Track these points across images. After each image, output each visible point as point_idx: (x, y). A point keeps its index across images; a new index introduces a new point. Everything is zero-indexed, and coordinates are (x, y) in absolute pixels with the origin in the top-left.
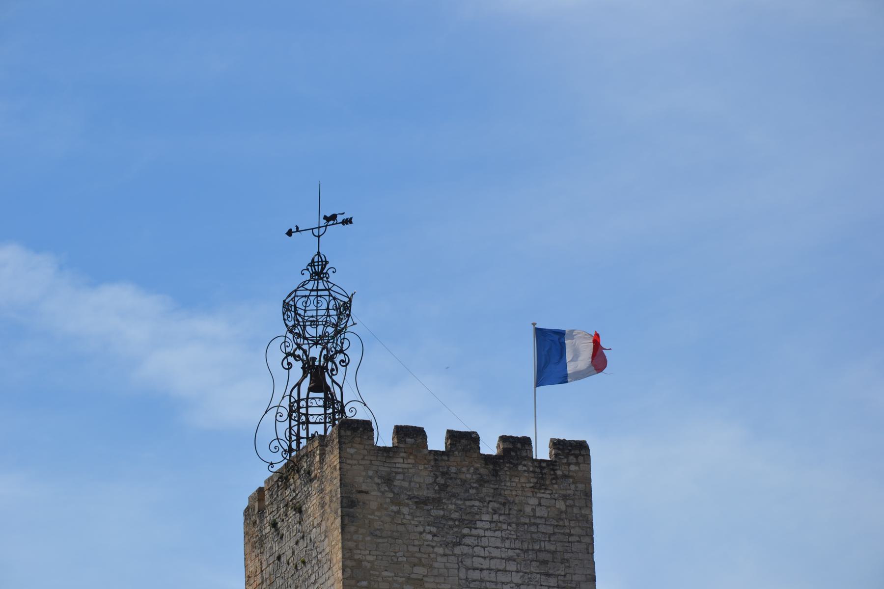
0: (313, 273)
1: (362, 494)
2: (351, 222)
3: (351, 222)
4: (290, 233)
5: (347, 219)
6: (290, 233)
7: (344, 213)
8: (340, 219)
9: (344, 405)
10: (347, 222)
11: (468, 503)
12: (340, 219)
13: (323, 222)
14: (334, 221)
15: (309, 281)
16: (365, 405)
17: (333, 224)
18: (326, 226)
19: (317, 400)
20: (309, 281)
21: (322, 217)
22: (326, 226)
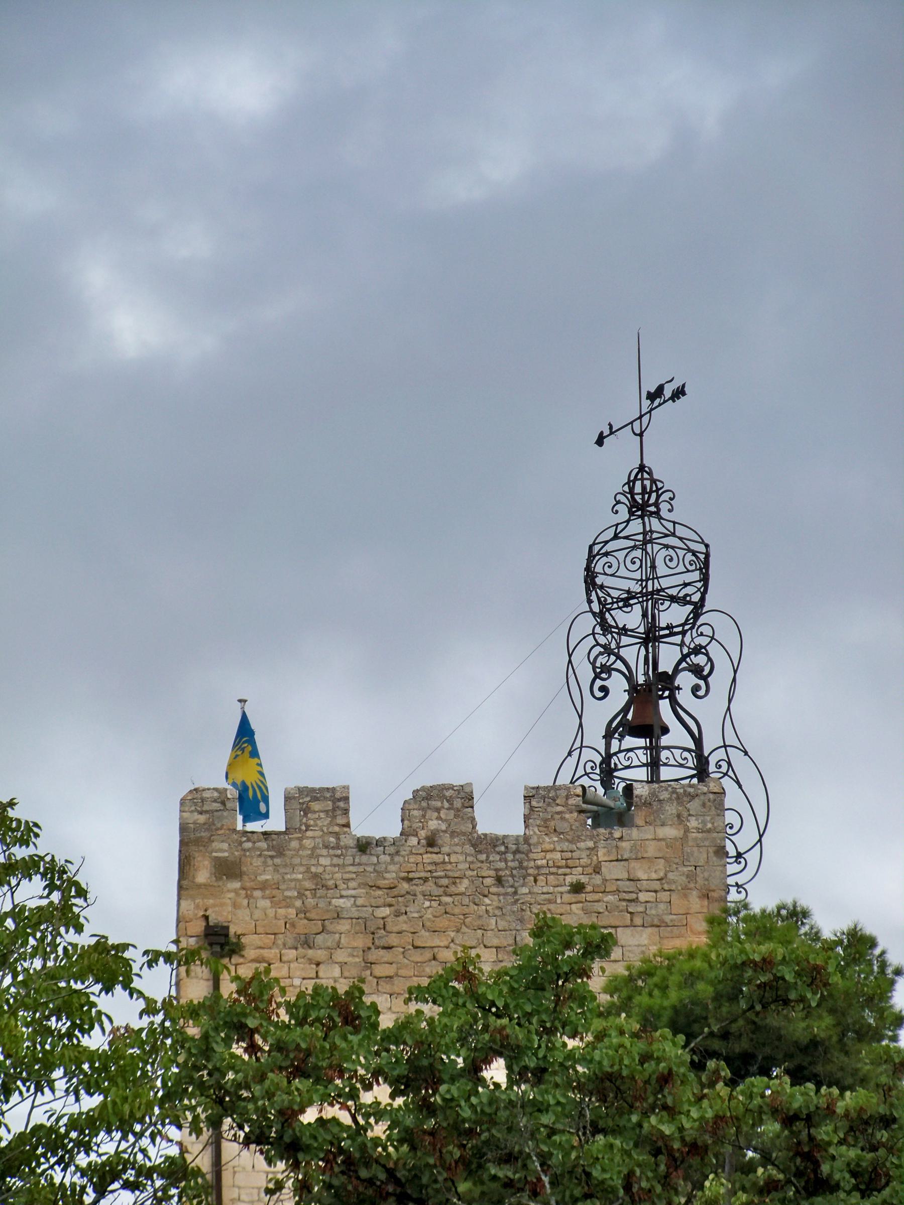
0: (632, 507)
1: (211, 983)
2: (684, 394)
3: (684, 394)
4: (600, 441)
5: (678, 388)
6: (600, 441)
7: (673, 378)
8: (668, 392)
9: (706, 754)
10: (679, 393)
11: (556, 889)
12: (668, 392)
13: (646, 403)
14: (661, 398)
15: (628, 521)
16: (746, 753)
17: (660, 405)
18: (650, 412)
19: (672, 762)
20: (628, 521)
21: (644, 395)
22: (650, 412)
